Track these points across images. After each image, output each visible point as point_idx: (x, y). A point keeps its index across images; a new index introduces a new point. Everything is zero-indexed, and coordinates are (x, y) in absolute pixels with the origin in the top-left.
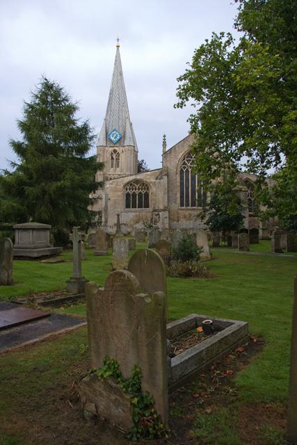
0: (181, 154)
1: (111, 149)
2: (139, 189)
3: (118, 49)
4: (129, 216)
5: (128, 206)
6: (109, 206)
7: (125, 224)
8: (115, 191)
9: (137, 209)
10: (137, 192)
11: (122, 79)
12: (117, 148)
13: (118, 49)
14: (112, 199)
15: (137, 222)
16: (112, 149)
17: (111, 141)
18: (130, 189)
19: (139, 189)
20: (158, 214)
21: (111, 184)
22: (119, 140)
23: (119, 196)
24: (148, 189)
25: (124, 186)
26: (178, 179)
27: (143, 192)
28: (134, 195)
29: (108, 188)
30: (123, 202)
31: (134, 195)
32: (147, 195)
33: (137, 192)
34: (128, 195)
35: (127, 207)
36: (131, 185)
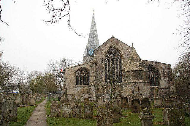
0: (105, 50)
1: (90, 58)
2: (84, 73)
3: (93, 14)
4: (79, 89)
5: (77, 84)
6: (67, 83)
7: (71, 95)
8: (70, 75)
9: (83, 85)
10: (83, 75)
11: (95, 26)
12: (92, 57)
13: (93, 14)
14: (68, 79)
15: (82, 93)
16: (90, 58)
17: (89, 54)
18: (79, 74)
19: (84, 73)
20: (91, 88)
21: (68, 71)
22: (93, 54)
23: (73, 78)
24: (89, 73)
25: (75, 72)
26: (104, 66)
27: (86, 75)
28: (81, 77)
29: (66, 73)
30: (74, 81)
31: (81, 77)
32: (88, 77)
33: (83, 75)
34: (78, 77)
35: (77, 84)
36: (80, 71)
